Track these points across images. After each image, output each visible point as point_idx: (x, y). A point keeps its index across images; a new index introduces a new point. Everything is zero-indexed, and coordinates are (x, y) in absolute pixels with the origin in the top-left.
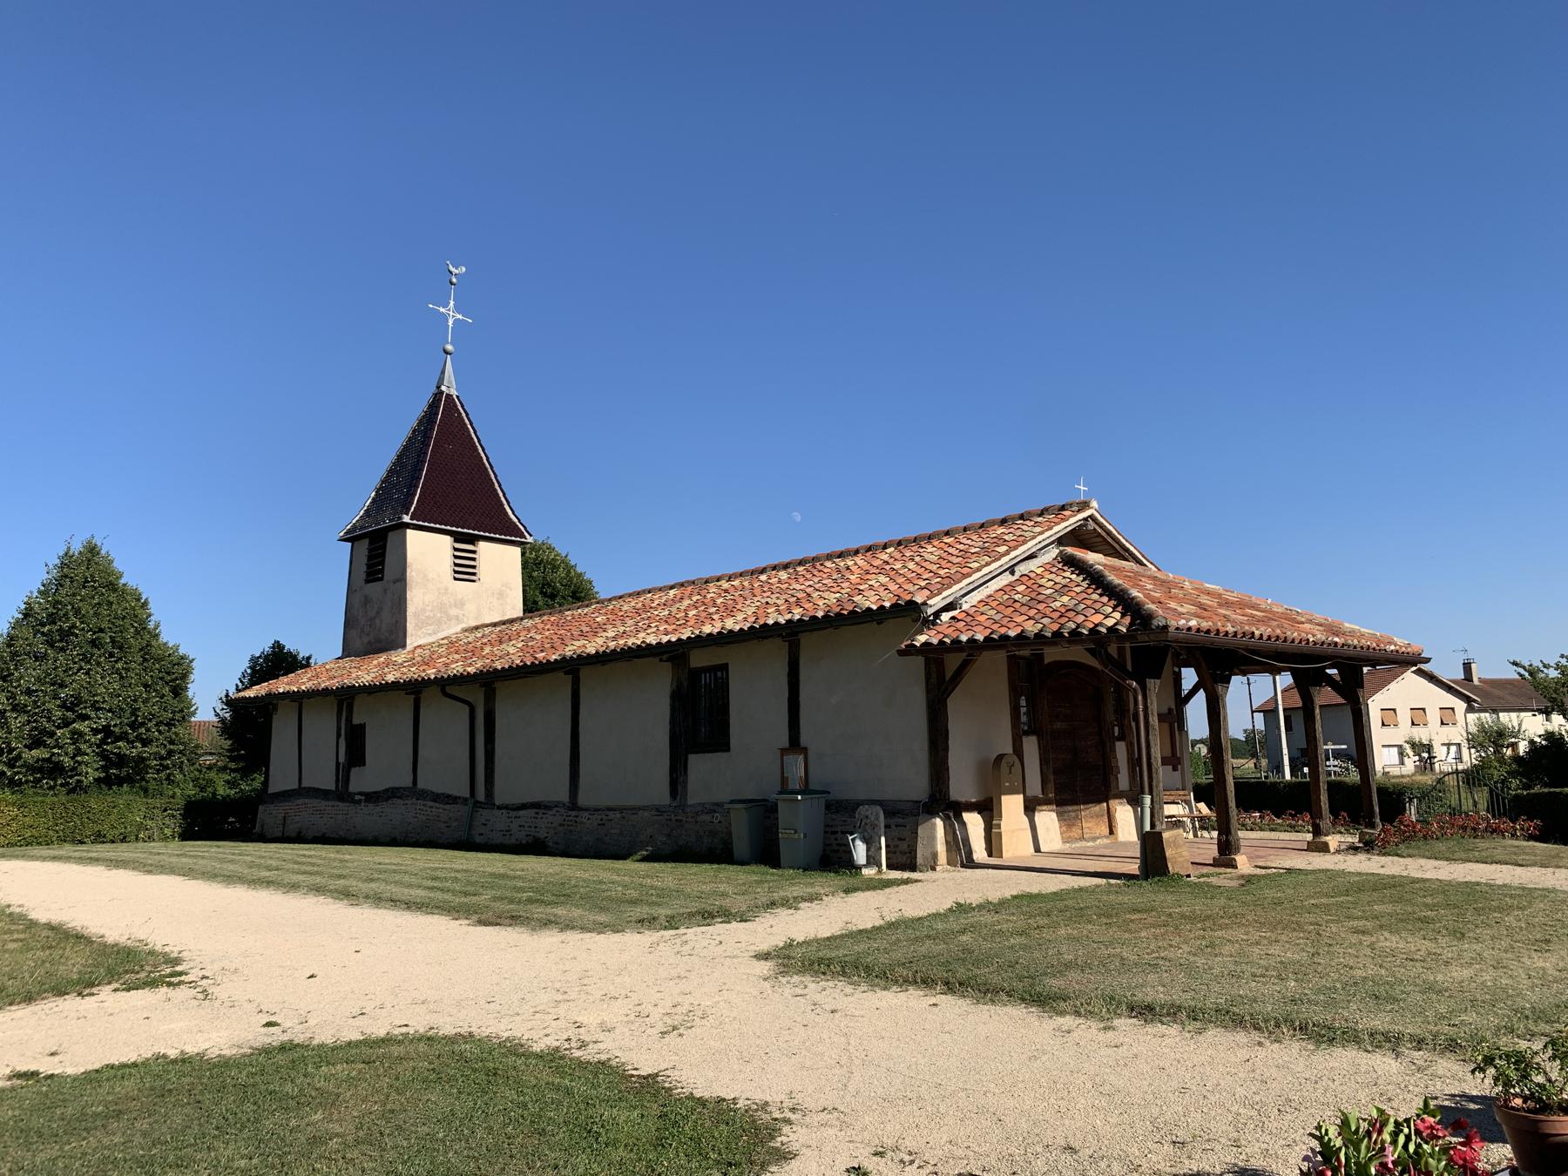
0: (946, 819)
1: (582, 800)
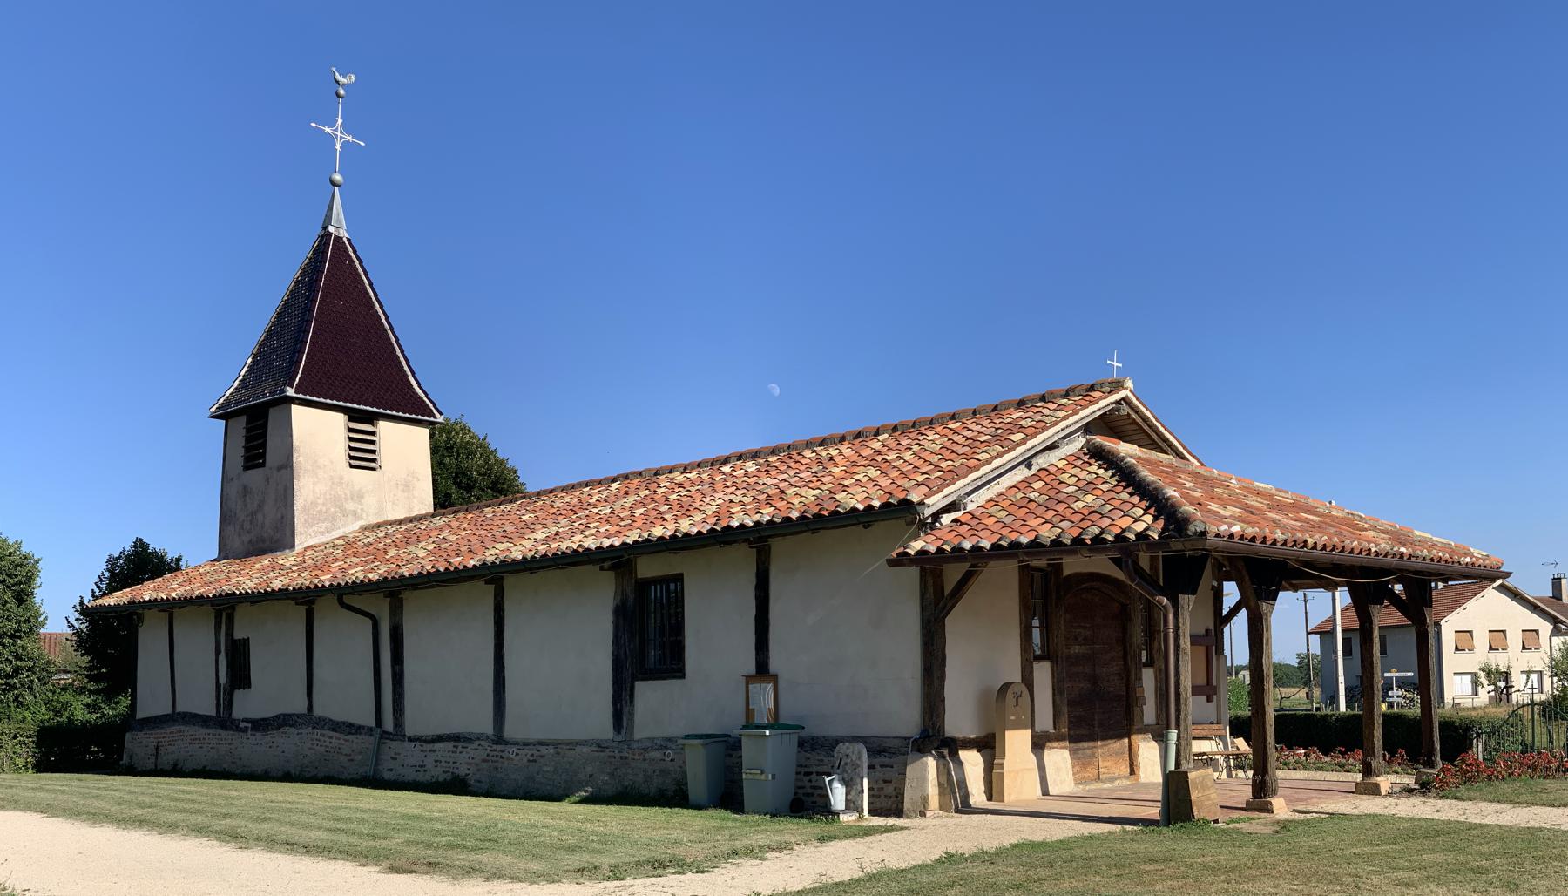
0: (940, 757)
1: (510, 732)
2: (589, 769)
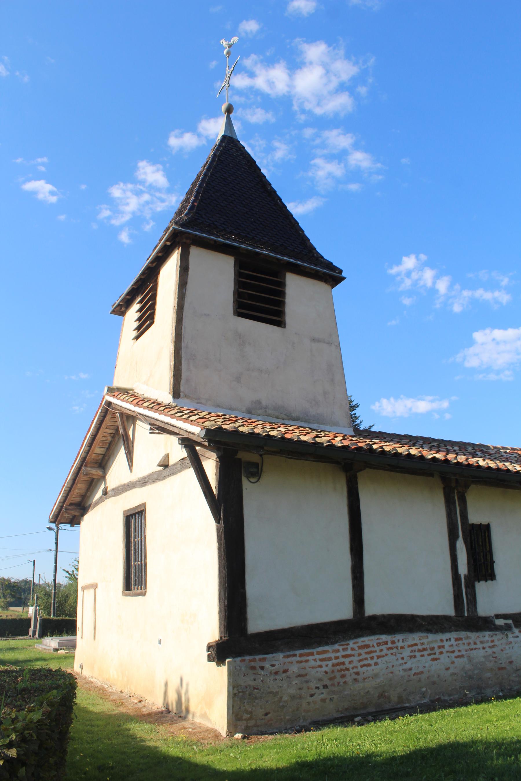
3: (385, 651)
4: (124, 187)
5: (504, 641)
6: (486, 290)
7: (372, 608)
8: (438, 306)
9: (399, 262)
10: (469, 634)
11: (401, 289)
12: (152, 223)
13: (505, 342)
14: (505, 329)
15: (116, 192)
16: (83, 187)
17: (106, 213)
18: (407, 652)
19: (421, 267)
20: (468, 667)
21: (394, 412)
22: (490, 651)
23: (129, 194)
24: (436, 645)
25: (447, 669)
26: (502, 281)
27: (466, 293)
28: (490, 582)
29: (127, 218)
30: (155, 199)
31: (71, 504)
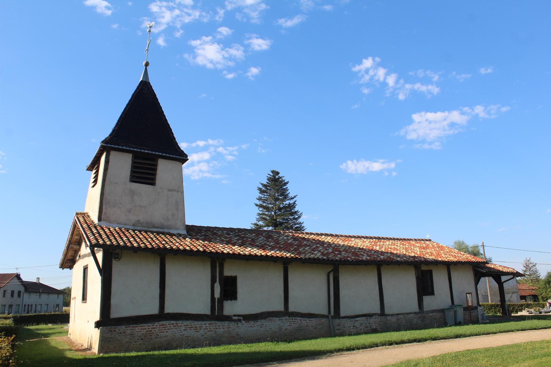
1: (387, 311)
2: (415, 320)
3: (172, 327)
4: (160, 4)
5: (236, 326)
6: (422, 84)
7: (291, 309)
8: (388, 95)
9: (360, 63)
10: (217, 322)
11: (361, 82)
12: (181, 32)
13: (435, 122)
14: (435, 112)
15: (154, 8)
16: (130, 4)
17: (147, 24)
18: (183, 328)
19: (377, 66)
20: (214, 335)
21: (356, 170)
22: (227, 330)
23: (164, 9)
24: (198, 326)
25: (203, 336)
26: (434, 77)
27: (408, 86)
28: (233, 301)
29: (163, 27)
30: (184, 14)
31: (68, 260)
